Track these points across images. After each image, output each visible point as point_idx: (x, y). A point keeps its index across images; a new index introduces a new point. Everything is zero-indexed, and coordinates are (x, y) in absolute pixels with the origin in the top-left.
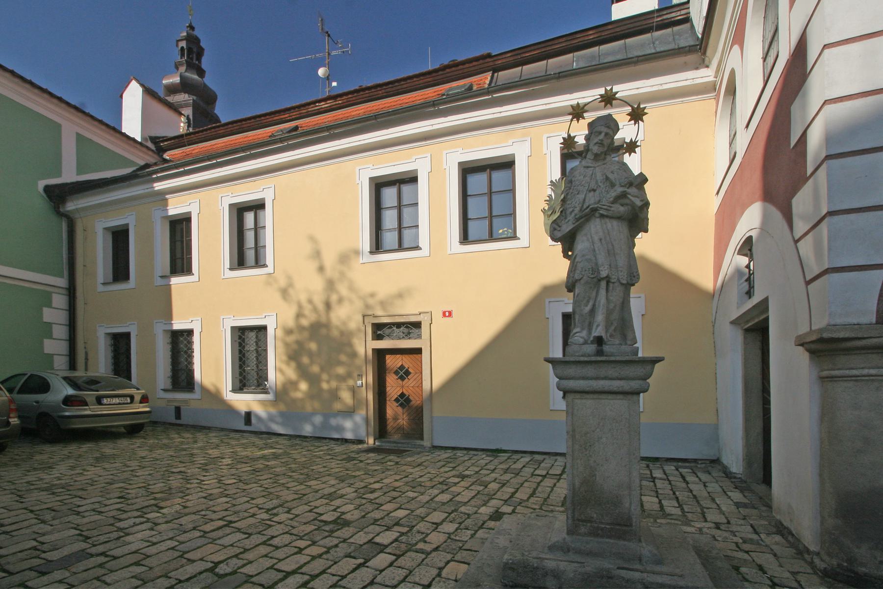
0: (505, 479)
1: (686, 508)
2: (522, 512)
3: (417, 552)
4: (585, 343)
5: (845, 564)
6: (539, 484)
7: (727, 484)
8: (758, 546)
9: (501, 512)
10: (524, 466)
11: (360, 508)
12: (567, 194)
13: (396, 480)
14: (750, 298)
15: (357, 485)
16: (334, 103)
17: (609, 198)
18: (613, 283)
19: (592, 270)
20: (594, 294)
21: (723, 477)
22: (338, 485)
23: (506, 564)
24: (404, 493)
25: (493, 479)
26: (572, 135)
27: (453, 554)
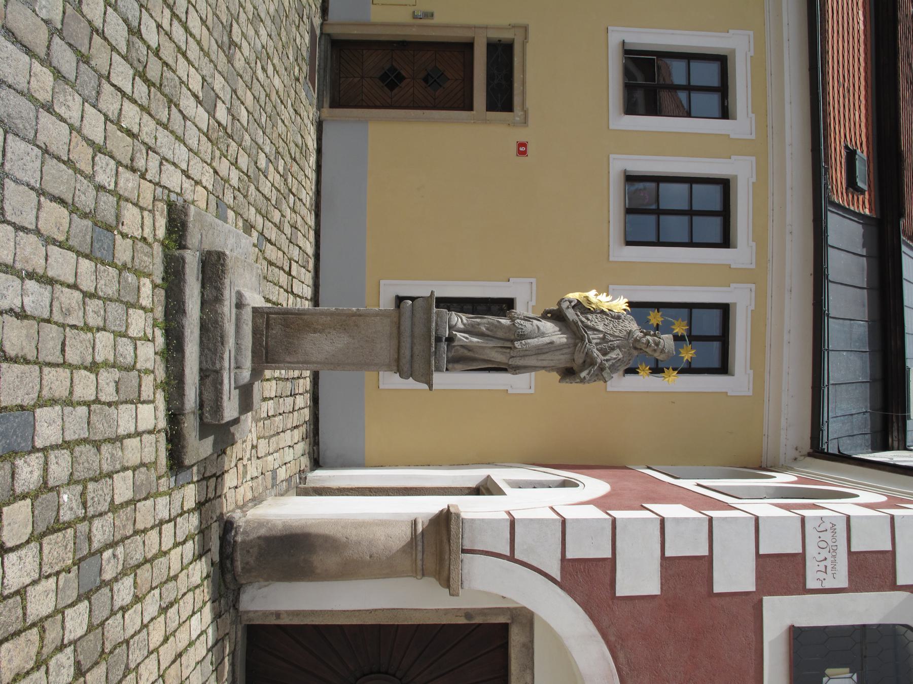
4: (451, 328)
5: (241, 530)
6: (282, 268)
10: (300, 248)
18: (510, 353)
25: (284, 214)
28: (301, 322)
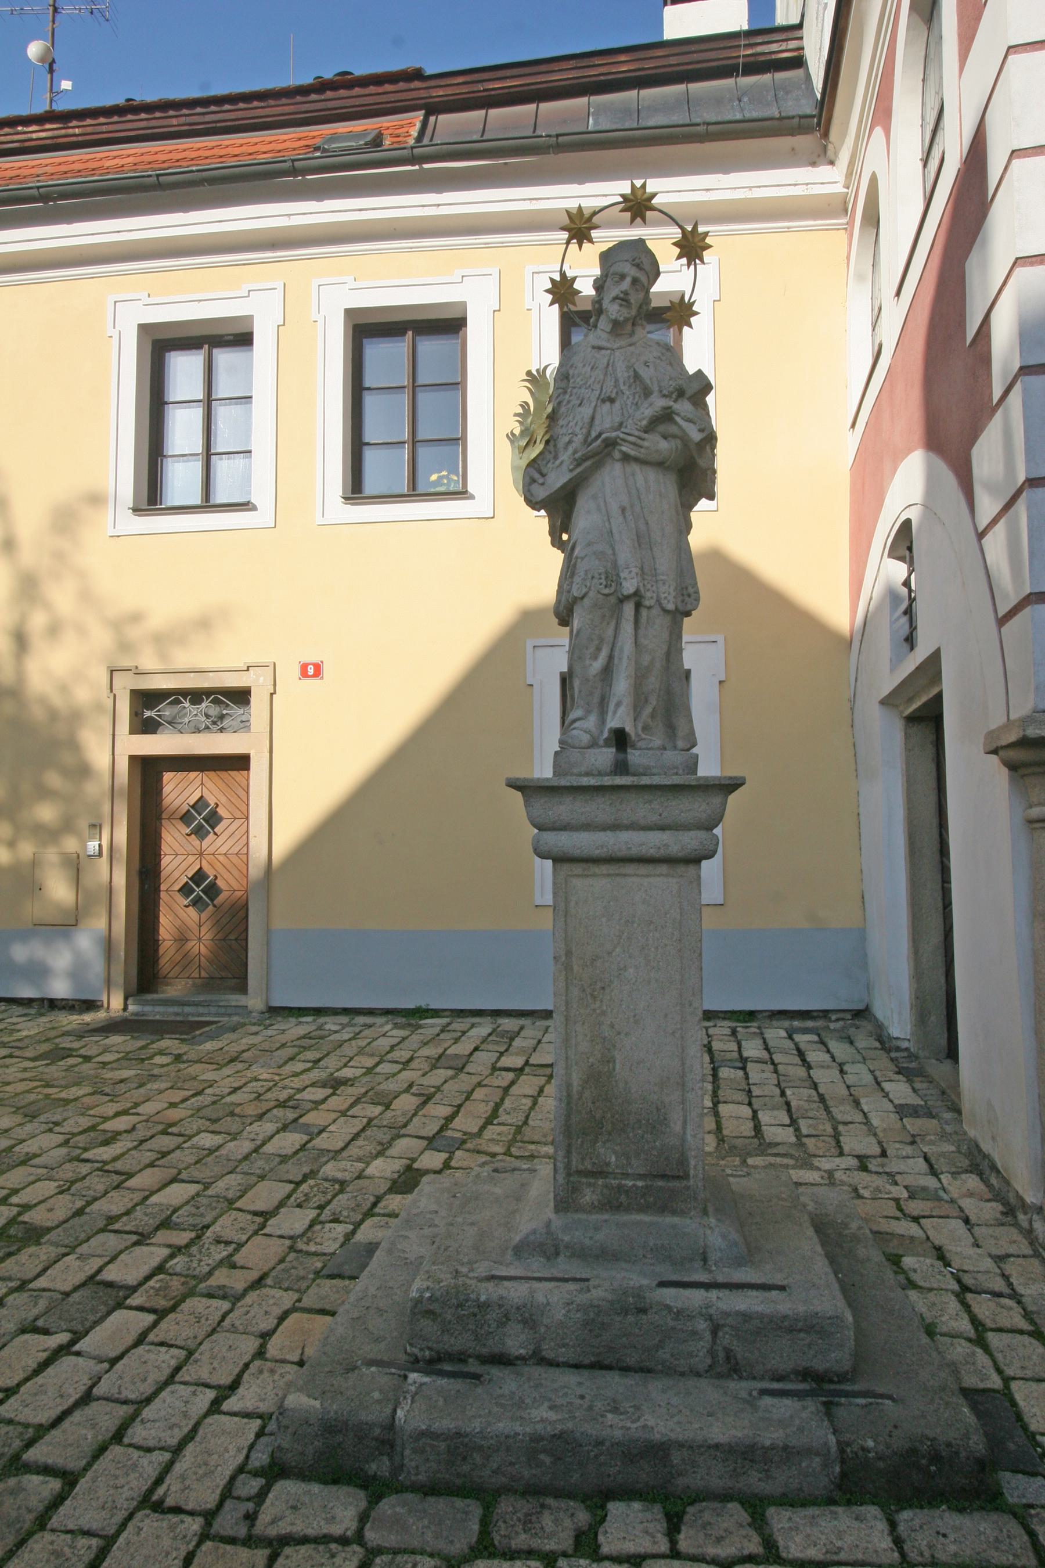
0: (432, 1083)
1: (804, 1127)
2: (465, 1164)
3: (210, 1296)
4: (593, 744)
6: (506, 1090)
7: (882, 1063)
8: (937, 1203)
9: (417, 1170)
10: (476, 1049)
11: (73, 1190)
12: (559, 403)
13: (173, 1105)
14: (912, 649)
15: (69, 1127)
16: (63, 132)
17: (640, 421)
18: (649, 608)
19: (607, 578)
20: (610, 632)
21: (876, 1049)
22: (18, 1130)
23: (418, 1302)
24: (190, 1137)
25: (406, 1085)
26: (570, 274)
27: (298, 1291)
28: (587, 1094)
